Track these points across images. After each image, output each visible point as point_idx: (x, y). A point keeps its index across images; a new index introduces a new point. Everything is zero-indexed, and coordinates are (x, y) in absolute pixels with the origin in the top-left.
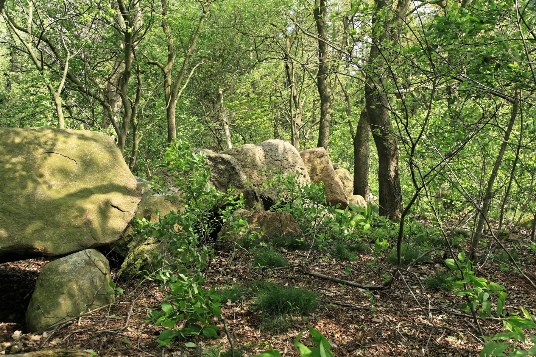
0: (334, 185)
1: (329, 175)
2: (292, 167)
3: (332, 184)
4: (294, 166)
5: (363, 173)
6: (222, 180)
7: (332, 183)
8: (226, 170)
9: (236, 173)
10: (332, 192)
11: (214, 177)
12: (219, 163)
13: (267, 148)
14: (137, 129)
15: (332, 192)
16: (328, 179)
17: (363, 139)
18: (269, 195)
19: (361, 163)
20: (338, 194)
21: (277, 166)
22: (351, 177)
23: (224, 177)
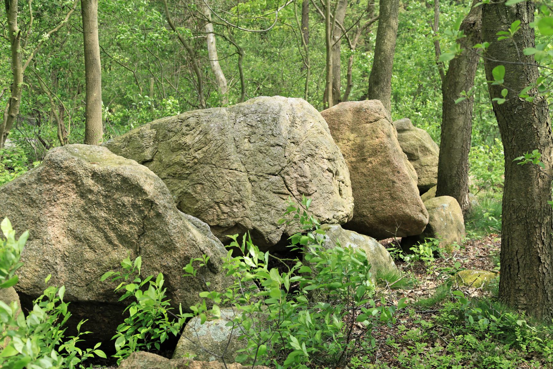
0: (399, 184)
1: (389, 162)
2: (309, 159)
3: (394, 182)
4: (311, 155)
5: (458, 147)
6: (125, 228)
7: (395, 179)
8: (134, 205)
9: (158, 215)
10: (393, 199)
11: (106, 220)
12: (117, 189)
13: (252, 119)
14: (20, 44)
15: (393, 199)
16: (387, 170)
17: (462, 80)
18: (257, 224)
19: (456, 128)
20: (405, 203)
21: (274, 158)
22: (435, 149)
23: (129, 223)
